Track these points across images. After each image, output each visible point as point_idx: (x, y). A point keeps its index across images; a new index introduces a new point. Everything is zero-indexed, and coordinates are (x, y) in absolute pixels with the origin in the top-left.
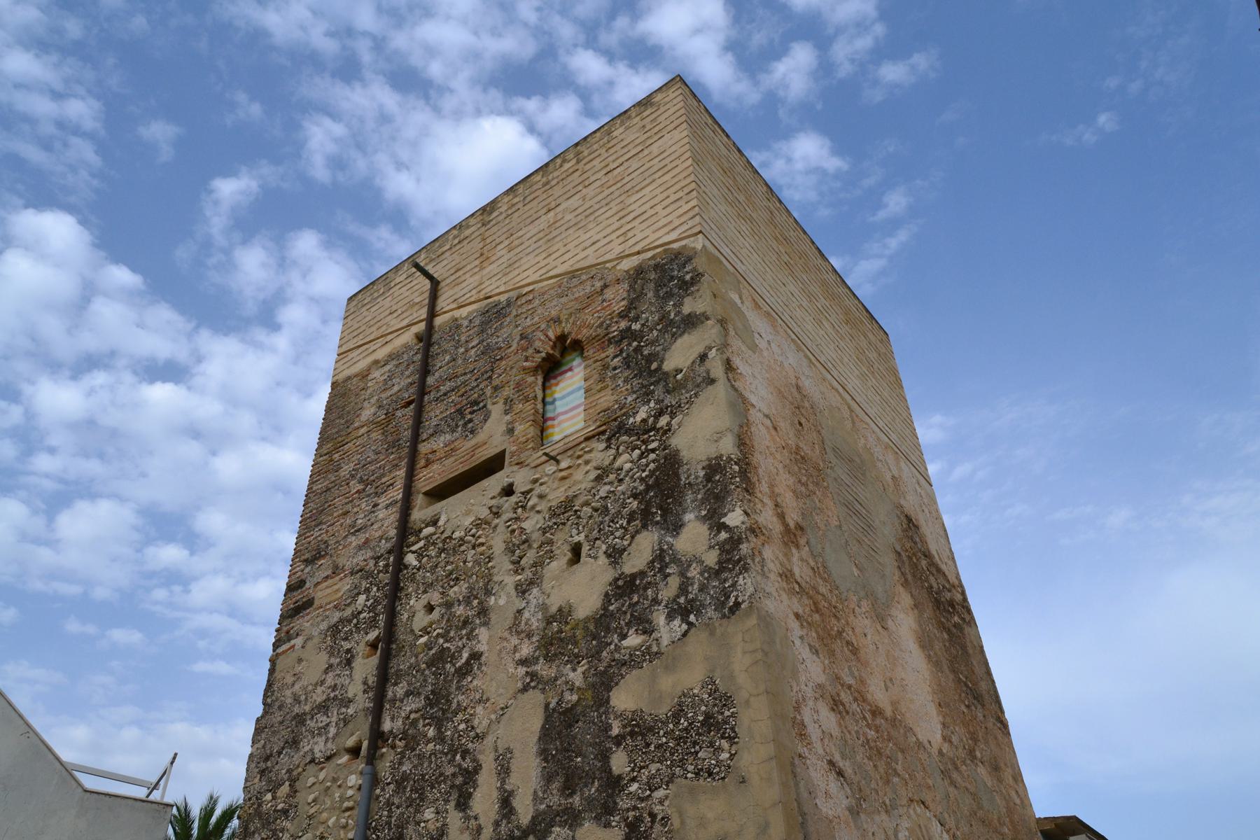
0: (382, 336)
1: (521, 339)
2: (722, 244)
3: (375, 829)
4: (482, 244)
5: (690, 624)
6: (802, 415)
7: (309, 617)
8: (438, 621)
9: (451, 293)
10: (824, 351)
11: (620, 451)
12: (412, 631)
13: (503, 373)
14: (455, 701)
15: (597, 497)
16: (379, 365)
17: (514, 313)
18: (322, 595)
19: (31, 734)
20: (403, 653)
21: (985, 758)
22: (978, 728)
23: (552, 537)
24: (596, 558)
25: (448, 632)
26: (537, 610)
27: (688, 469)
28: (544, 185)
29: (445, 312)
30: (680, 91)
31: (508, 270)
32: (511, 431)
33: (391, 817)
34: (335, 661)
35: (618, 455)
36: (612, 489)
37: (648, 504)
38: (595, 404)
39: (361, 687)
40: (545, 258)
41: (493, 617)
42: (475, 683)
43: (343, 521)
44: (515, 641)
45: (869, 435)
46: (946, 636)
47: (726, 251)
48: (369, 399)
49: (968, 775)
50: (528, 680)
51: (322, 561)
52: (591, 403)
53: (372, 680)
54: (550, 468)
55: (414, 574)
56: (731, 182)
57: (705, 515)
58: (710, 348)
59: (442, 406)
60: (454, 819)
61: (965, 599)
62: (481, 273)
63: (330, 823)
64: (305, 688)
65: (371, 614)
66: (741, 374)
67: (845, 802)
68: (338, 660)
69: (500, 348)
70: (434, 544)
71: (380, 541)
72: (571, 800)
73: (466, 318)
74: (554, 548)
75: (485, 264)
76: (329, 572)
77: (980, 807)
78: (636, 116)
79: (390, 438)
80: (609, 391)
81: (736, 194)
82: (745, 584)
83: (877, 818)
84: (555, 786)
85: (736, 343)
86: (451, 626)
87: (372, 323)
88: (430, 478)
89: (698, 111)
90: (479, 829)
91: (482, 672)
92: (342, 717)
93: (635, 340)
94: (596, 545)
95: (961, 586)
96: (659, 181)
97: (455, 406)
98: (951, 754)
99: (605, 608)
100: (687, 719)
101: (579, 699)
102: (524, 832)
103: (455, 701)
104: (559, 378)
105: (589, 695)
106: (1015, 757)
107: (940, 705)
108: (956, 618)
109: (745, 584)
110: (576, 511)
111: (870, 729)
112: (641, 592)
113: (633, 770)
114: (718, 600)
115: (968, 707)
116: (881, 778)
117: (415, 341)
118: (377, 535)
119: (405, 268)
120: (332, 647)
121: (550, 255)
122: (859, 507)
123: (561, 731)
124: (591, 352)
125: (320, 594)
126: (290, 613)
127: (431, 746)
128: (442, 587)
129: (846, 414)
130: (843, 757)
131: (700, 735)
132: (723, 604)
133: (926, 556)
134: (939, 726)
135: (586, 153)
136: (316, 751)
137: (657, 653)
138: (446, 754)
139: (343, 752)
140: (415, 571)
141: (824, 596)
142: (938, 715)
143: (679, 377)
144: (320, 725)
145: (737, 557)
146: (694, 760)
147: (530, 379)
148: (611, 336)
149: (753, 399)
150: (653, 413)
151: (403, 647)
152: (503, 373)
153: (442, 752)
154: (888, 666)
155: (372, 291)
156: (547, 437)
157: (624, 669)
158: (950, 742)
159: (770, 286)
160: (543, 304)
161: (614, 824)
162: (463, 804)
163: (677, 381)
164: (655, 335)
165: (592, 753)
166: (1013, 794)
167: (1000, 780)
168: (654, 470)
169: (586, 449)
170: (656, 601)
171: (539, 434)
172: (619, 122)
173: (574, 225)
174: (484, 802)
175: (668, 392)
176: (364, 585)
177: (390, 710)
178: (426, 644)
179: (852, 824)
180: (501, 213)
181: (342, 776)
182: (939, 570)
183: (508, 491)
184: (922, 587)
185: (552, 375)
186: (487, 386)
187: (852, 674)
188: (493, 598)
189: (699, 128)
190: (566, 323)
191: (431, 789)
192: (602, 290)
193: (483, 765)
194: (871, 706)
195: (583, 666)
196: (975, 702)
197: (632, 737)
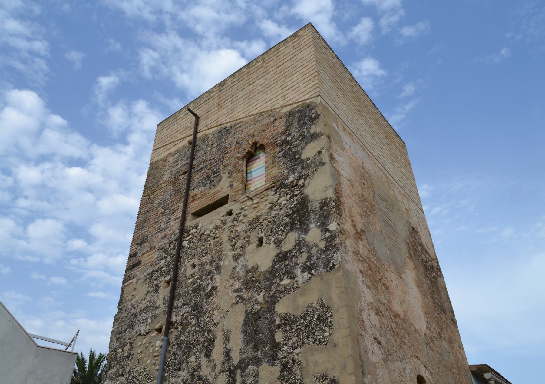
0: (173, 142)
3: (168, 365)
4: (219, 100)
5: (312, 275)
6: (365, 180)
7: (139, 269)
8: (198, 272)
9: (204, 122)
10: (376, 151)
11: (281, 195)
12: (186, 276)
14: (205, 308)
16: (172, 155)
17: (233, 132)
18: (145, 260)
19: (14, 321)
22: (443, 324)
23: (249, 234)
24: (269, 244)
25: (202, 277)
26: (242, 267)
27: (312, 204)
28: (248, 73)
29: (202, 131)
30: (310, 30)
31: (231, 112)
32: (231, 186)
33: (175, 360)
34: (150, 289)
36: (277, 213)
37: (294, 220)
39: (162, 301)
40: (248, 107)
41: (222, 270)
42: (214, 300)
43: (154, 226)
44: (232, 281)
46: (429, 282)
47: (331, 104)
50: (238, 299)
51: (145, 244)
52: (268, 173)
53: (167, 298)
54: (249, 203)
55: (186, 250)
56: (334, 73)
57: (320, 225)
58: (323, 149)
60: (204, 361)
61: (438, 265)
62: (218, 113)
63: (148, 362)
64: (137, 301)
65: (167, 268)
66: (337, 161)
67: (381, 356)
68: (152, 289)
69: (227, 148)
70: (196, 237)
71: (171, 235)
73: (211, 134)
74: (250, 239)
75: (220, 109)
76: (148, 249)
77: (443, 360)
79: (176, 189)
81: (336, 78)
82: (337, 256)
83: (396, 364)
84: (250, 347)
85: (335, 147)
86: (203, 274)
87: (168, 136)
90: (215, 366)
91: (217, 295)
92: (153, 315)
93: (289, 145)
94: (269, 238)
95: (437, 259)
97: (206, 174)
98: (430, 336)
99: (273, 267)
100: (310, 317)
101: (261, 308)
104: (254, 162)
106: (460, 337)
107: (426, 313)
108: (434, 274)
109: (337, 256)
110: (261, 223)
111: (393, 323)
112: (290, 260)
113: (285, 340)
115: (438, 314)
116: (398, 345)
117: (188, 144)
118: (170, 232)
119: (184, 111)
120: (149, 283)
121: (250, 105)
122: (390, 222)
124: (268, 150)
126: (130, 267)
127: (194, 328)
128: (200, 256)
129: (385, 180)
130: (381, 336)
131: (316, 325)
132: (327, 265)
133: (420, 245)
134: (425, 323)
135: (267, 59)
136: (142, 330)
137: (296, 287)
138: (201, 332)
139: (154, 330)
140: (187, 249)
141: (373, 262)
143: (308, 162)
144: (144, 318)
145: (334, 244)
146: (313, 336)
147: (241, 162)
148: (277, 143)
149: (342, 172)
150: (296, 178)
151: (182, 283)
152: (228, 159)
153: (199, 331)
154: (402, 295)
155: (169, 121)
156: (248, 189)
157: (281, 294)
158: (430, 330)
159: (351, 121)
160: (247, 128)
161: (276, 364)
163: (307, 164)
164: (298, 142)
165: (267, 332)
166: (458, 354)
167: (453, 348)
168: (297, 204)
169: (266, 194)
170: (296, 264)
171: (244, 187)
172: (282, 44)
173: (261, 91)
174: (218, 353)
175: (303, 169)
178: (192, 282)
179: (384, 366)
180: (228, 86)
181: (154, 341)
182: (426, 252)
183: (230, 213)
184: (419, 259)
185: (250, 160)
186: (221, 165)
187: (385, 298)
188: (222, 262)
190: (257, 136)
191: (194, 347)
192: (274, 122)
194: (394, 313)
195: (263, 293)
196: (442, 312)
197: (285, 325)
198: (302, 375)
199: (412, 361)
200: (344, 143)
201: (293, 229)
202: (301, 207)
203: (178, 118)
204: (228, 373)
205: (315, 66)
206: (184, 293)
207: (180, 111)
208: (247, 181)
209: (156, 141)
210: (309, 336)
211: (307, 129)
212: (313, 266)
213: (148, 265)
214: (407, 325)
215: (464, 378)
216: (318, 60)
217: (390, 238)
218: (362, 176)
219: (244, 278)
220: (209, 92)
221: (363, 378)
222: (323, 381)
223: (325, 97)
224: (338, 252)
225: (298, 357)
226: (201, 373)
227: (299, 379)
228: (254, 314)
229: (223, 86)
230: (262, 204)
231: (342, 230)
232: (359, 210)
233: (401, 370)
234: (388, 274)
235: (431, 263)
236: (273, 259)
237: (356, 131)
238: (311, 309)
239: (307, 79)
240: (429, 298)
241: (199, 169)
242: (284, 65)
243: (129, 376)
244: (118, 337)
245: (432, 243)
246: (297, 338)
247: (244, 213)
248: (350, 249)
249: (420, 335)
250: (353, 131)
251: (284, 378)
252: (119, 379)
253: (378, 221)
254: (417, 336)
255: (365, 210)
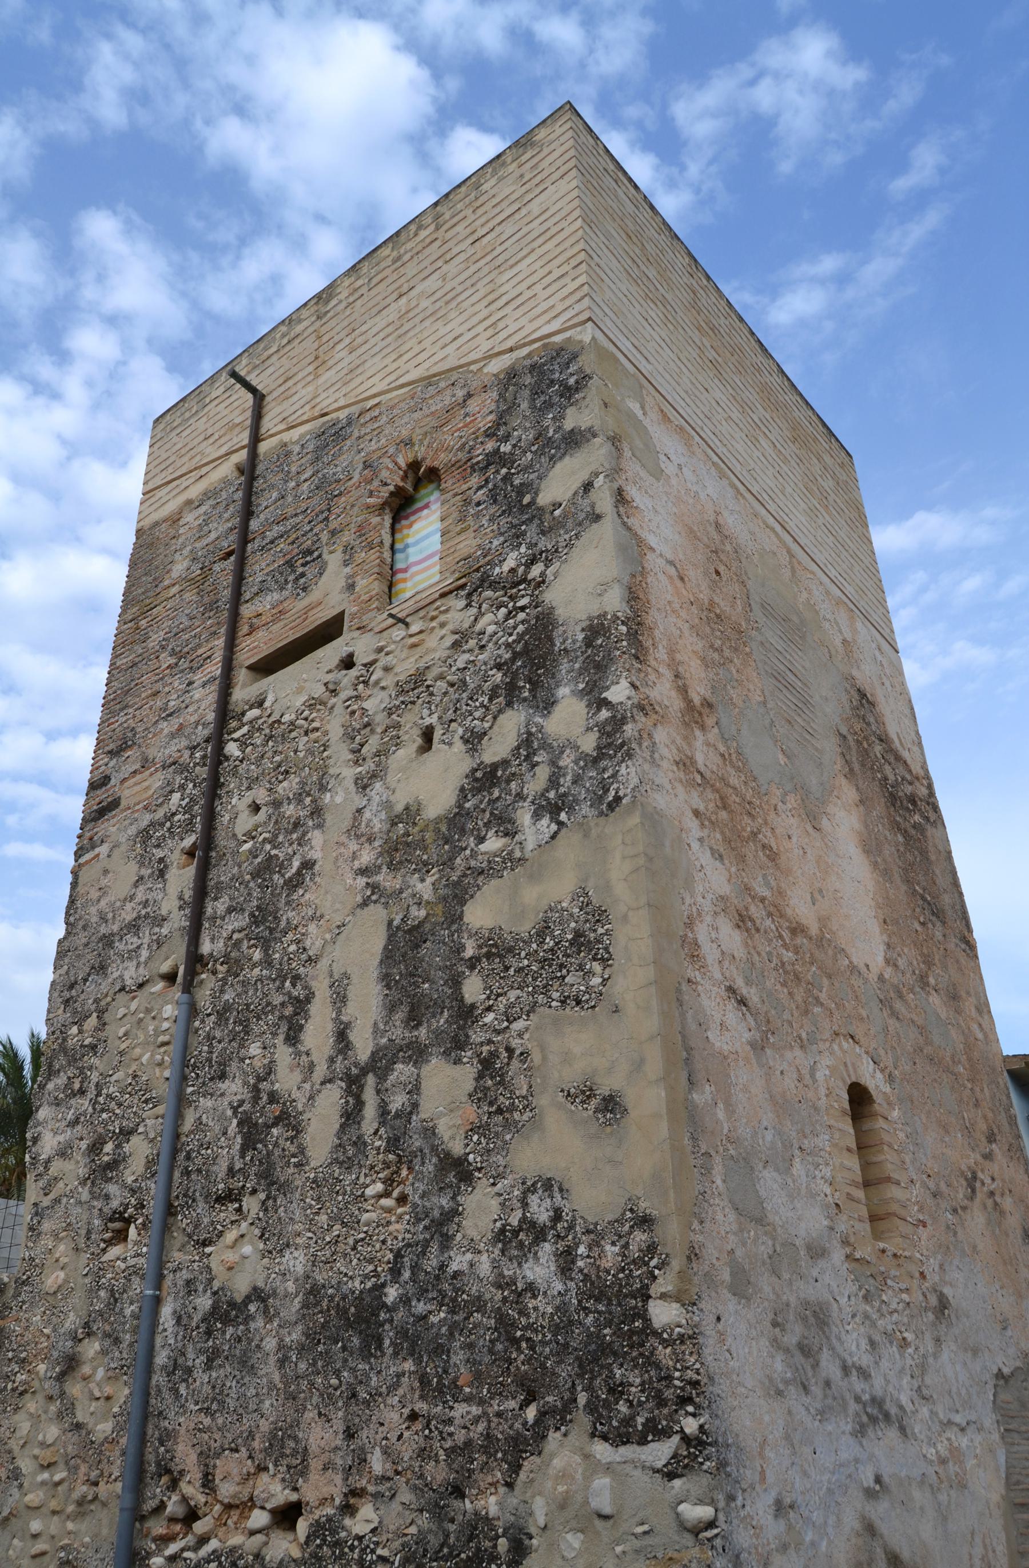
0: (196, 469)
1: (365, 469)
2: (621, 337)
3: (194, 1066)
4: (317, 343)
5: (561, 824)
6: (721, 561)
7: (115, 820)
8: (265, 823)
9: (278, 410)
10: (759, 479)
11: (483, 610)
12: (234, 835)
13: (342, 513)
14: (284, 918)
15: (454, 669)
16: (193, 506)
17: (356, 434)
18: (129, 794)
20: (224, 862)
21: (940, 986)
23: (399, 719)
24: (450, 744)
25: (276, 836)
26: (380, 808)
27: (565, 632)
28: (394, 261)
29: (272, 436)
30: (569, 124)
31: (349, 377)
32: (351, 587)
33: (211, 1052)
34: (146, 872)
35: (480, 614)
36: (472, 658)
37: (515, 676)
38: (452, 550)
39: (177, 903)
40: (394, 361)
41: (329, 817)
42: (307, 896)
43: (152, 703)
44: (353, 846)
45: (814, 587)
46: (901, 839)
47: (625, 344)
48: (181, 550)
49: (916, 1007)
51: (129, 753)
52: (448, 549)
53: (188, 894)
54: (399, 632)
55: (236, 766)
56: (637, 251)
57: (583, 689)
58: (597, 475)
59: (268, 557)
60: (283, 1054)
61: (932, 794)
62: (315, 382)
63: (144, 1059)
64: (112, 904)
65: (187, 816)
66: (637, 508)
67: (747, 1036)
68: (149, 871)
69: (338, 481)
70: (259, 729)
71: (196, 728)
72: (416, 1033)
73: (297, 442)
74: (401, 733)
75: (320, 371)
76: (137, 766)
77: (929, 1042)
78: (513, 161)
79: (206, 600)
80: (470, 533)
81: (643, 268)
82: (628, 774)
83: (789, 1055)
84: (399, 1016)
85: (632, 467)
86: (279, 829)
87: (183, 451)
88: (255, 648)
89: (595, 152)
90: (312, 1066)
91: (315, 883)
92: (155, 937)
93: (504, 466)
94: (451, 729)
95: (928, 777)
96: (539, 252)
97: (284, 556)
98: (895, 981)
99: (460, 806)
100: (553, 938)
101: (428, 915)
102: (362, 1069)
103: (284, 918)
104: (412, 518)
105: (439, 909)
107: (885, 922)
108: (917, 818)
109: (628, 774)
110: (428, 687)
111: (787, 950)
112: (503, 785)
113: (489, 998)
114: (595, 794)
115: (923, 924)
116: (797, 1008)
117: (236, 474)
118: (193, 719)
119: (223, 379)
120: (142, 856)
121: (401, 356)
122: (794, 678)
123: (406, 953)
124: (450, 482)
125: (127, 793)
126: (93, 815)
127: (257, 971)
128: (269, 782)
129: (784, 558)
130: (748, 983)
131: (568, 956)
132: (601, 798)
133: (881, 740)
134: (882, 947)
135: (447, 216)
136: (126, 977)
137: (520, 859)
138: (274, 980)
140: (237, 763)
141: (735, 789)
142: (882, 934)
143: (557, 513)
144: (131, 947)
145: (620, 741)
146: (560, 985)
147: (375, 520)
148: (474, 461)
149: (652, 540)
150: (523, 561)
151: (224, 854)
152: (342, 513)
153: (270, 978)
154: (818, 874)
155: (183, 410)
156: (397, 594)
157: (481, 878)
158: (895, 965)
159: (687, 392)
160: (391, 421)
162: (293, 1038)
163: (554, 518)
164: (529, 459)
165: (441, 978)
166: (975, 1027)
167: (958, 1011)
168: (523, 632)
169: (442, 609)
170: (520, 796)
171: (387, 590)
172: (490, 170)
173: (431, 314)
175: (543, 533)
176: (177, 782)
177: (209, 929)
178: (250, 851)
179: (754, 1061)
180: (341, 301)
181: (157, 1007)
182: (898, 758)
183: (348, 663)
184: (873, 779)
185: (403, 514)
186: (323, 530)
187: (767, 884)
188: (328, 795)
189: (594, 175)
190: (420, 445)
191: (258, 1020)
192: (465, 401)
193: (316, 993)
194: (791, 922)
195: (433, 875)
196: (934, 919)
197: (488, 959)
198: (531, 1087)
199: (836, 1047)
200: (663, 458)
201: (513, 702)
202: (535, 640)
203: (207, 400)
204: (343, 1084)
205: (580, 232)
206: (231, 879)
207: (213, 379)
208: (393, 575)
209: (151, 466)
210: (551, 986)
211: (553, 418)
212: (563, 802)
213: (137, 808)
214: (826, 953)
215: (986, 1090)
216: (589, 213)
217: (790, 723)
218: (712, 551)
219: (385, 837)
220: (289, 321)
221: (690, 1092)
222: (583, 1102)
223: (607, 325)
224: (629, 763)
225: (520, 1041)
226: (277, 1086)
227: (523, 1097)
228: (410, 931)
229: (328, 302)
230: (433, 635)
231: (644, 703)
232: (699, 645)
233: (803, 1072)
234: (779, 819)
235: (910, 788)
236: (459, 785)
237: (700, 422)
238: (557, 915)
239: (557, 273)
240: (898, 881)
241: (265, 542)
242: (493, 235)
243: (99, 1094)
244: (68, 996)
245: (917, 733)
246: (519, 991)
247: (384, 661)
248: (667, 753)
249: (866, 981)
250: (692, 423)
251: (485, 1095)
252: (73, 1102)
253: (755, 674)
254: (856, 982)
255: (716, 646)
